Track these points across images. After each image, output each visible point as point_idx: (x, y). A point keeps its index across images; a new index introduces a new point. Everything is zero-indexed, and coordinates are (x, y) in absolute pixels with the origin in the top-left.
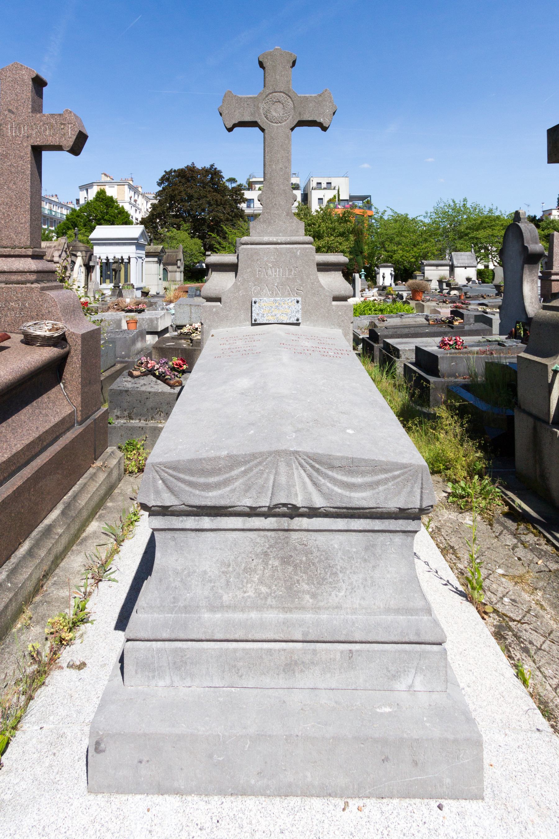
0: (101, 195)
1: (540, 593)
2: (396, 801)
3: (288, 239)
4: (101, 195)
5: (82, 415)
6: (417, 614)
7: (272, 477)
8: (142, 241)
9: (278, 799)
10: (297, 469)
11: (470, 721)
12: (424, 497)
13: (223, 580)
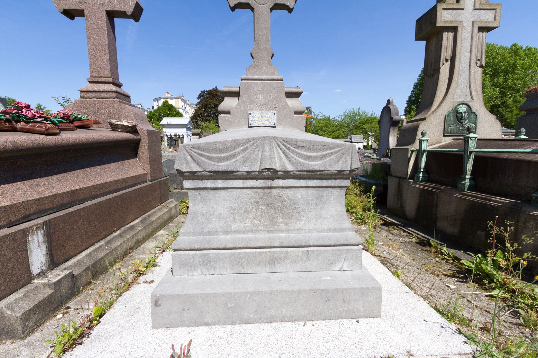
0: (166, 103)
1: (401, 250)
2: (333, 321)
4: (166, 104)
5: (151, 176)
6: (346, 231)
7: (260, 153)
8: (189, 126)
9: (266, 324)
10: (276, 148)
11: (374, 279)
12: (353, 163)
13: (231, 218)
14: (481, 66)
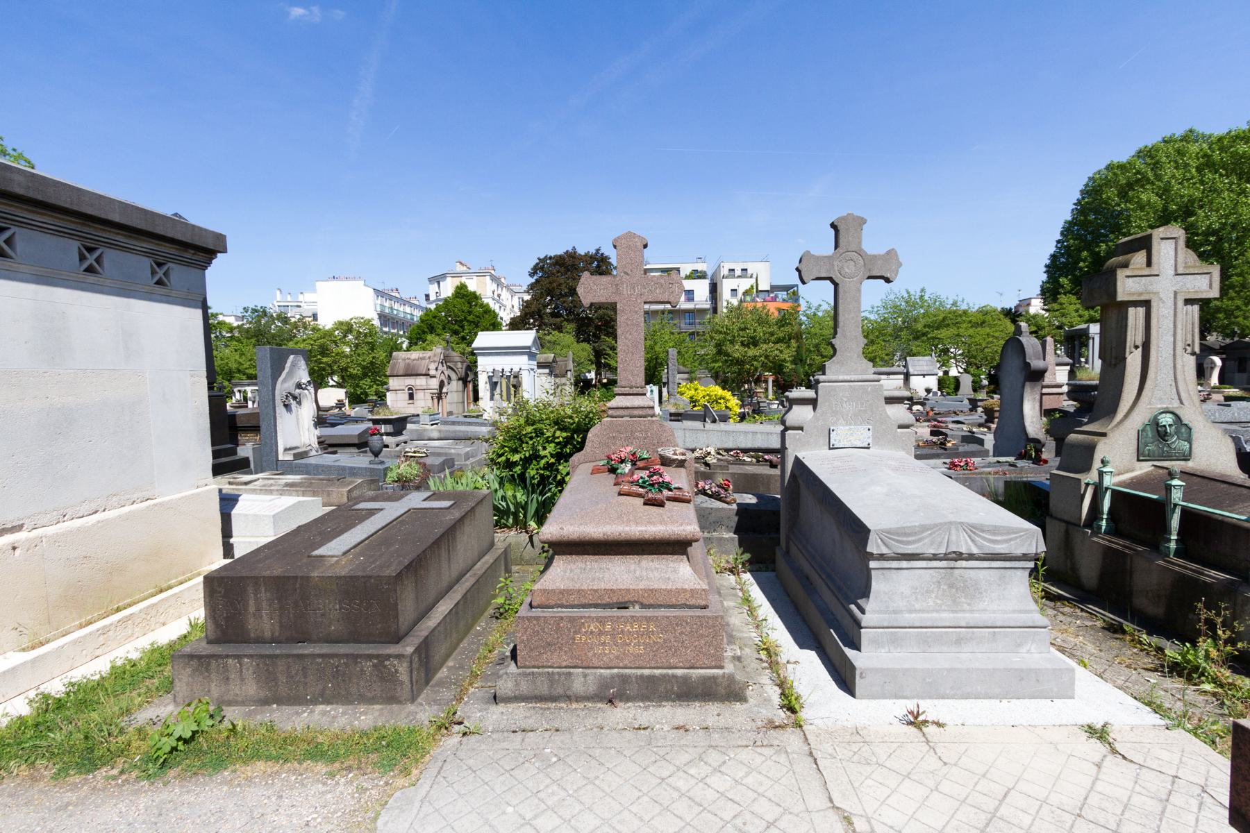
0: (461, 292)
3: (861, 377)
4: (461, 292)
14: (1193, 354)
